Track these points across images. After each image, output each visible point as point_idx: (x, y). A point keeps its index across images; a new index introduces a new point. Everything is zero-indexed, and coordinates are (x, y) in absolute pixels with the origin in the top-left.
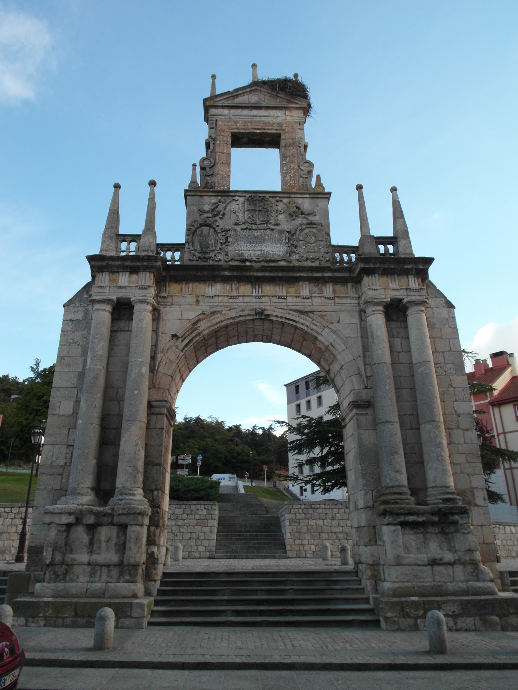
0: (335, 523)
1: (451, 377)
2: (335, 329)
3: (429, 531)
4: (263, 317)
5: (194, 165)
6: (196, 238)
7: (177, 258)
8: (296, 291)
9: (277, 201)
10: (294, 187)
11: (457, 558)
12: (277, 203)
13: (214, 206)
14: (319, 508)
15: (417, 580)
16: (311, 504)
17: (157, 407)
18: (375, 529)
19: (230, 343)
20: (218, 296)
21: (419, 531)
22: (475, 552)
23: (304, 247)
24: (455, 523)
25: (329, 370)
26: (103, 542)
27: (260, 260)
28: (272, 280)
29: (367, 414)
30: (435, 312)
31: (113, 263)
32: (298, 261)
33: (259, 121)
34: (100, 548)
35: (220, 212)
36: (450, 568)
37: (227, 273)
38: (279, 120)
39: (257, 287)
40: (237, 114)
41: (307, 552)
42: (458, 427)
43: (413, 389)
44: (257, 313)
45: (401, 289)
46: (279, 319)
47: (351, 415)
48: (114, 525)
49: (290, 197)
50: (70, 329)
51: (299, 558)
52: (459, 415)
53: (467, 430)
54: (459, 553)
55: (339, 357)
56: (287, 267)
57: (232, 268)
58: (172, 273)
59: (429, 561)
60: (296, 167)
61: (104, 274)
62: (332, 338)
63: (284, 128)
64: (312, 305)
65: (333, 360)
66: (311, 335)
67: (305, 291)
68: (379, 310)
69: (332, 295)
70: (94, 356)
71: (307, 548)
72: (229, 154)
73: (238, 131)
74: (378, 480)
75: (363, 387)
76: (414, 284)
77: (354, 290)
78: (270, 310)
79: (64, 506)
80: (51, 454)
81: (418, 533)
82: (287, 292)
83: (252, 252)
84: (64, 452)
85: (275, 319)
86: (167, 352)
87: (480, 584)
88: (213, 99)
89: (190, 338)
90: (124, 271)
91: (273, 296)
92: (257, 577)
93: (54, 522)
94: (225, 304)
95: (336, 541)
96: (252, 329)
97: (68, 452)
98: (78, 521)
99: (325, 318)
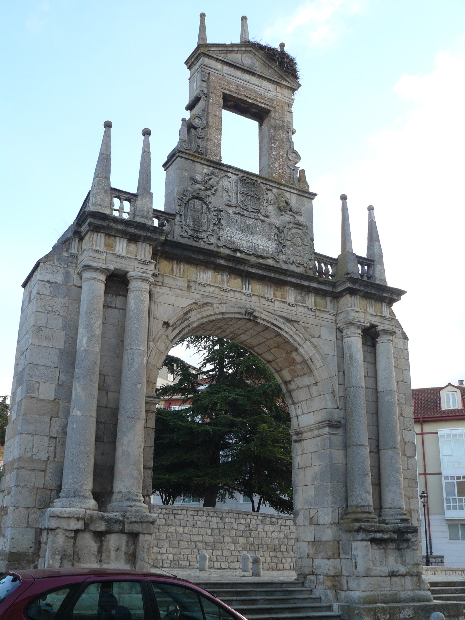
0: (195, 531)
2: (316, 343)
4: (252, 318)
8: (282, 295)
9: (268, 190)
11: (408, 570)
13: (207, 178)
14: (181, 514)
15: (379, 589)
16: (173, 510)
18: (339, 544)
20: (211, 285)
21: (382, 547)
22: (420, 566)
23: (291, 249)
26: (112, 551)
27: (251, 253)
28: (262, 279)
31: (114, 226)
32: (285, 262)
33: (252, 89)
34: (109, 557)
35: (213, 187)
36: (402, 578)
37: (222, 262)
38: (270, 95)
41: (164, 561)
44: (247, 313)
46: (265, 323)
49: (279, 188)
50: (48, 294)
52: (405, 443)
55: (316, 372)
57: (228, 258)
58: (167, 249)
59: (389, 573)
61: (122, 241)
62: (312, 352)
63: (274, 106)
64: (296, 314)
65: (304, 374)
67: (290, 298)
68: (358, 333)
69: (294, 303)
70: (92, 336)
71: (164, 557)
73: (230, 93)
75: (336, 407)
77: (332, 306)
80: (31, 445)
81: (381, 549)
82: (275, 296)
83: (244, 242)
84: (46, 444)
85: (261, 322)
86: (158, 341)
87: (422, 593)
89: (180, 328)
90: (122, 237)
91: (262, 297)
92: (217, 588)
94: (216, 296)
95: (195, 550)
97: (51, 445)
99: (308, 330)
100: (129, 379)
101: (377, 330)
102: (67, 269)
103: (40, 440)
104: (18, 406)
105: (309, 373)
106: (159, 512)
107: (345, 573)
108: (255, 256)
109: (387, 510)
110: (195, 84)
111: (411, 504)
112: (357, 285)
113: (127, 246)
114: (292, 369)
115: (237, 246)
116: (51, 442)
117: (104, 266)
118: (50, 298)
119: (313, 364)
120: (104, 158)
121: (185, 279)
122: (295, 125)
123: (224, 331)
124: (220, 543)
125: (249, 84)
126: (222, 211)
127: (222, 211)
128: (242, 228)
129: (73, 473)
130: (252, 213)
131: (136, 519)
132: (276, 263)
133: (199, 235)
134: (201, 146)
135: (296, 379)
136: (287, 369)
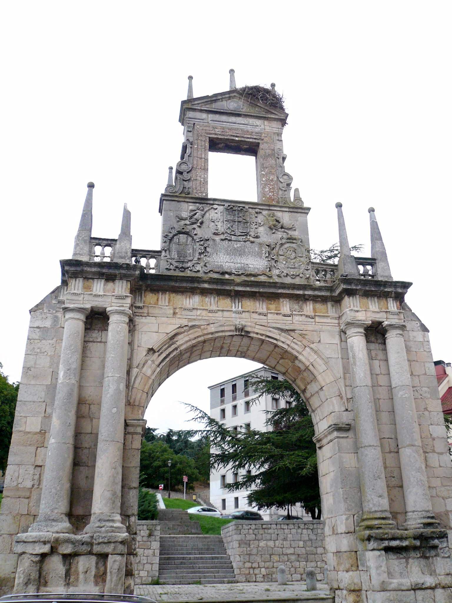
1: (427, 401)
2: (315, 349)
3: (411, 555)
4: (243, 334)
5: (171, 168)
6: (174, 247)
7: (152, 266)
8: (276, 307)
10: (273, 200)
11: (437, 582)
12: (256, 215)
16: (262, 525)
17: (133, 426)
19: (202, 358)
20: (197, 309)
21: (402, 556)
23: (284, 262)
24: (435, 547)
25: (305, 389)
27: (240, 273)
28: (252, 295)
29: (348, 437)
30: (410, 335)
31: (89, 269)
32: (279, 276)
34: (77, 579)
35: (198, 220)
37: (206, 286)
38: (257, 130)
39: (237, 301)
40: (215, 119)
42: (434, 451)
43: (392, 411)
45: (381, 311)
47: (329, 438)
48: (93, 554)
49: (269, 210)
51: (249, 582)
52: (434, 439)
53: (442, 454)
54: (440, 577)
55: (319, 378)
57: (212, 281)
60: (275, 179)
61: (77, 280)
62: (313, 357)
63: (263, 138)
65: (312, 381)
66: (292, 355)
67: (285, 309)
69: (313, 314)
72: (206, 160)
73: (216, 136)
74: (361, 504)
75: (344, 409)
76: (393, 308)
77: (334, 309)
78: (251, 327)
79: (38, 533)
81: (401, 558)
82: (268, 309)
83: (233, 265)
84: (31, 472)
85: (255, 335)
88: (192, 102)
89: (167, 352)
91: (253, 312)
93: (27, 552)
94: (204, 318)
95: (288, 563)
96: (229, 344)
98: (53, 550)
99: (306, 337)
101: (384, 326)
103: (25, 470)
106: (249, 528)
107: (364, 588)
108: (245, 276)
109: (410, 514)
111: (447, 505)
112: (353, 285)
113: (104, 285)
115: (226, 269)
116: (36, 471)
117: (82, 306)
118: (39, 341)
119: (316, 369)
121: (171, 307)
122: (286, 151)
124: (313, 554)
125: (235, 125)
126: (208, 240)
127: (208, 240)
130: (240, 237)
131: (103, 539)
132: (269, 279)
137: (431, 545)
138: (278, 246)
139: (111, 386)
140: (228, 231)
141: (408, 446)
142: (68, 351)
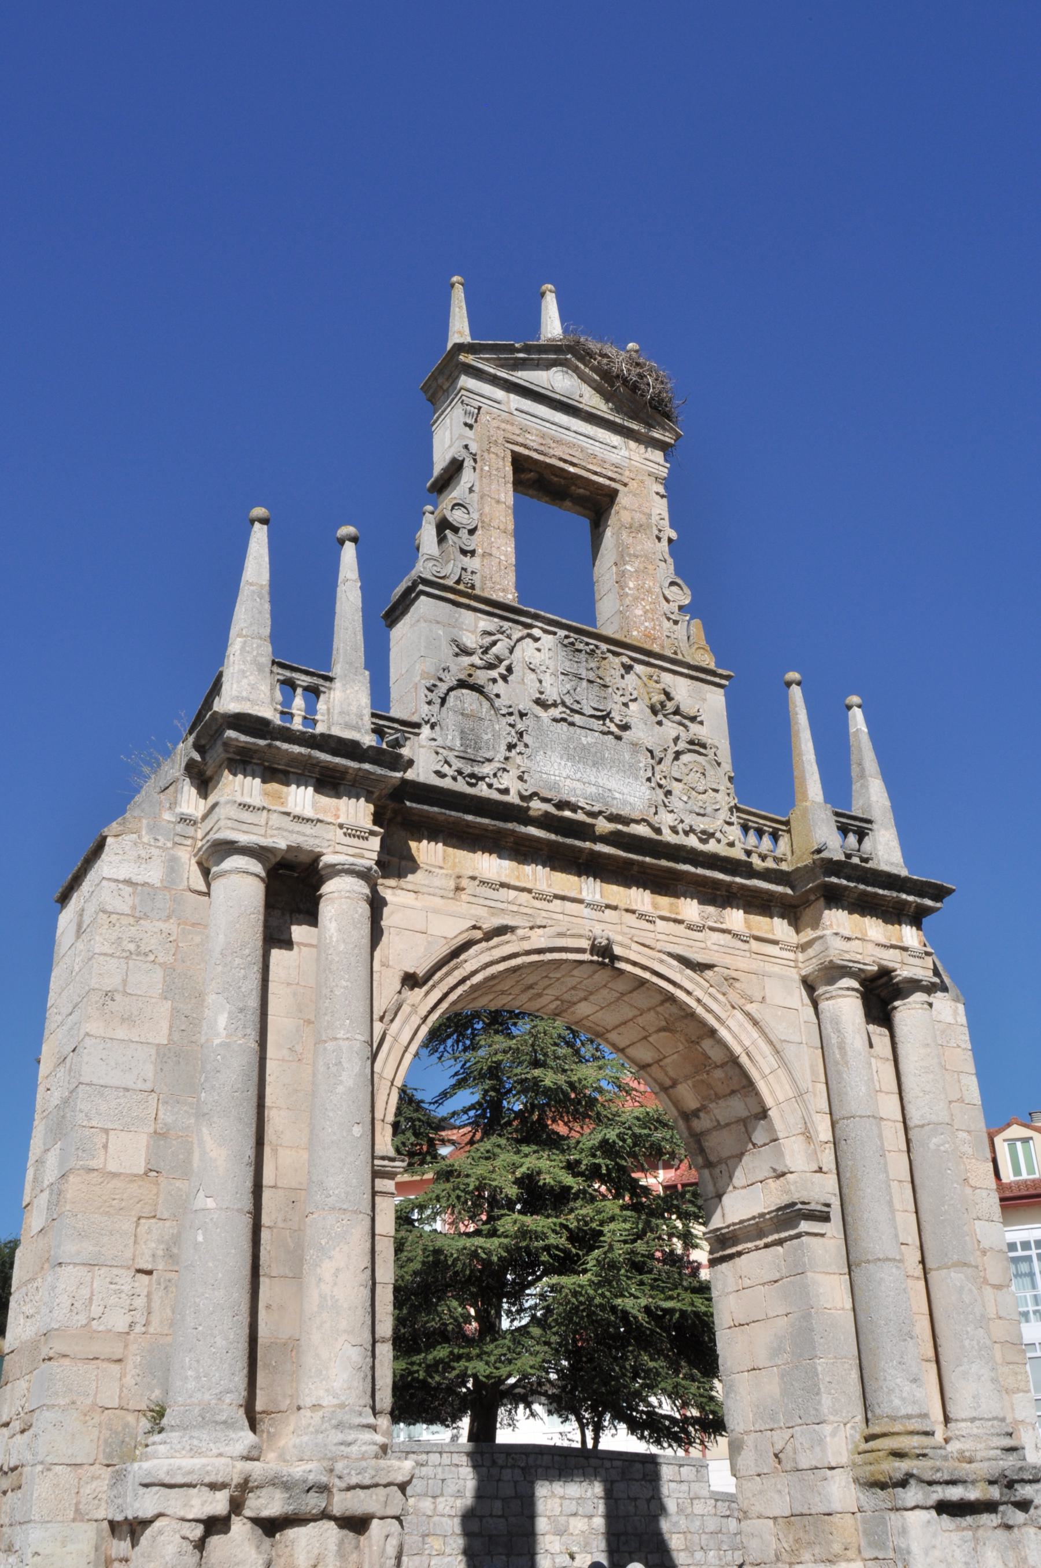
2: (757, 1016)
6: (449, 718)
23: (685, 798)
27: (596, 809)
38: (614, 457)
44: (595, 949)
50: (127, 911)
56: (650, 841)
63: (626, 480)
78: (622, 945)
80: (85, 1292)
81: (964, 1529)
83: (579, 785)
84: (126, 1288)
85: (628, 968)
97: (137, 1291)
99: (737, 985)
100: (331, 1114)
102: (172, 852)
103: (108, 1280)
104: (51, 1194)
105: (744, 1087)
109: (963, 1425)
110: (448, 433)
114: (702, 1081)
118: (132, 920)
119: (755, 1065)
120: (253, 592)
123: (540, 995)
125: (567, 432)
128: (571, 752)
129: (198, 1361)
131: (360, 1477)
133: (477, 770)
134: (469, 570)
135: (712, 1106)
136: (690, 1082)
137: (1018, 1499)
138: (670, 756)
139: (345, 1065)
140: (567, 700)
141: (955, 1265)
142: (238, 961)
